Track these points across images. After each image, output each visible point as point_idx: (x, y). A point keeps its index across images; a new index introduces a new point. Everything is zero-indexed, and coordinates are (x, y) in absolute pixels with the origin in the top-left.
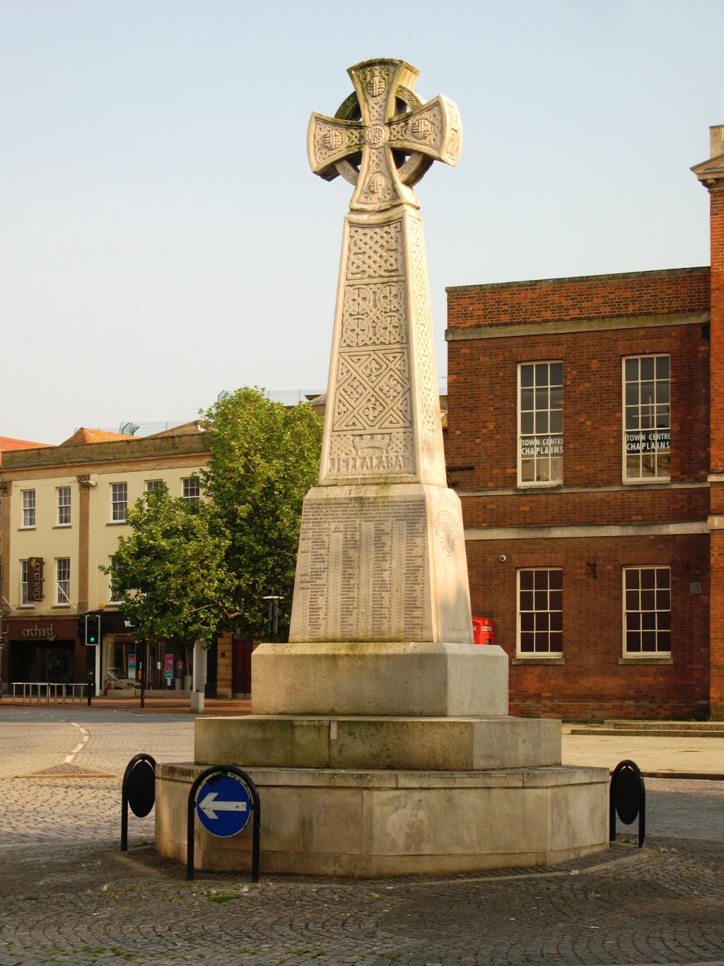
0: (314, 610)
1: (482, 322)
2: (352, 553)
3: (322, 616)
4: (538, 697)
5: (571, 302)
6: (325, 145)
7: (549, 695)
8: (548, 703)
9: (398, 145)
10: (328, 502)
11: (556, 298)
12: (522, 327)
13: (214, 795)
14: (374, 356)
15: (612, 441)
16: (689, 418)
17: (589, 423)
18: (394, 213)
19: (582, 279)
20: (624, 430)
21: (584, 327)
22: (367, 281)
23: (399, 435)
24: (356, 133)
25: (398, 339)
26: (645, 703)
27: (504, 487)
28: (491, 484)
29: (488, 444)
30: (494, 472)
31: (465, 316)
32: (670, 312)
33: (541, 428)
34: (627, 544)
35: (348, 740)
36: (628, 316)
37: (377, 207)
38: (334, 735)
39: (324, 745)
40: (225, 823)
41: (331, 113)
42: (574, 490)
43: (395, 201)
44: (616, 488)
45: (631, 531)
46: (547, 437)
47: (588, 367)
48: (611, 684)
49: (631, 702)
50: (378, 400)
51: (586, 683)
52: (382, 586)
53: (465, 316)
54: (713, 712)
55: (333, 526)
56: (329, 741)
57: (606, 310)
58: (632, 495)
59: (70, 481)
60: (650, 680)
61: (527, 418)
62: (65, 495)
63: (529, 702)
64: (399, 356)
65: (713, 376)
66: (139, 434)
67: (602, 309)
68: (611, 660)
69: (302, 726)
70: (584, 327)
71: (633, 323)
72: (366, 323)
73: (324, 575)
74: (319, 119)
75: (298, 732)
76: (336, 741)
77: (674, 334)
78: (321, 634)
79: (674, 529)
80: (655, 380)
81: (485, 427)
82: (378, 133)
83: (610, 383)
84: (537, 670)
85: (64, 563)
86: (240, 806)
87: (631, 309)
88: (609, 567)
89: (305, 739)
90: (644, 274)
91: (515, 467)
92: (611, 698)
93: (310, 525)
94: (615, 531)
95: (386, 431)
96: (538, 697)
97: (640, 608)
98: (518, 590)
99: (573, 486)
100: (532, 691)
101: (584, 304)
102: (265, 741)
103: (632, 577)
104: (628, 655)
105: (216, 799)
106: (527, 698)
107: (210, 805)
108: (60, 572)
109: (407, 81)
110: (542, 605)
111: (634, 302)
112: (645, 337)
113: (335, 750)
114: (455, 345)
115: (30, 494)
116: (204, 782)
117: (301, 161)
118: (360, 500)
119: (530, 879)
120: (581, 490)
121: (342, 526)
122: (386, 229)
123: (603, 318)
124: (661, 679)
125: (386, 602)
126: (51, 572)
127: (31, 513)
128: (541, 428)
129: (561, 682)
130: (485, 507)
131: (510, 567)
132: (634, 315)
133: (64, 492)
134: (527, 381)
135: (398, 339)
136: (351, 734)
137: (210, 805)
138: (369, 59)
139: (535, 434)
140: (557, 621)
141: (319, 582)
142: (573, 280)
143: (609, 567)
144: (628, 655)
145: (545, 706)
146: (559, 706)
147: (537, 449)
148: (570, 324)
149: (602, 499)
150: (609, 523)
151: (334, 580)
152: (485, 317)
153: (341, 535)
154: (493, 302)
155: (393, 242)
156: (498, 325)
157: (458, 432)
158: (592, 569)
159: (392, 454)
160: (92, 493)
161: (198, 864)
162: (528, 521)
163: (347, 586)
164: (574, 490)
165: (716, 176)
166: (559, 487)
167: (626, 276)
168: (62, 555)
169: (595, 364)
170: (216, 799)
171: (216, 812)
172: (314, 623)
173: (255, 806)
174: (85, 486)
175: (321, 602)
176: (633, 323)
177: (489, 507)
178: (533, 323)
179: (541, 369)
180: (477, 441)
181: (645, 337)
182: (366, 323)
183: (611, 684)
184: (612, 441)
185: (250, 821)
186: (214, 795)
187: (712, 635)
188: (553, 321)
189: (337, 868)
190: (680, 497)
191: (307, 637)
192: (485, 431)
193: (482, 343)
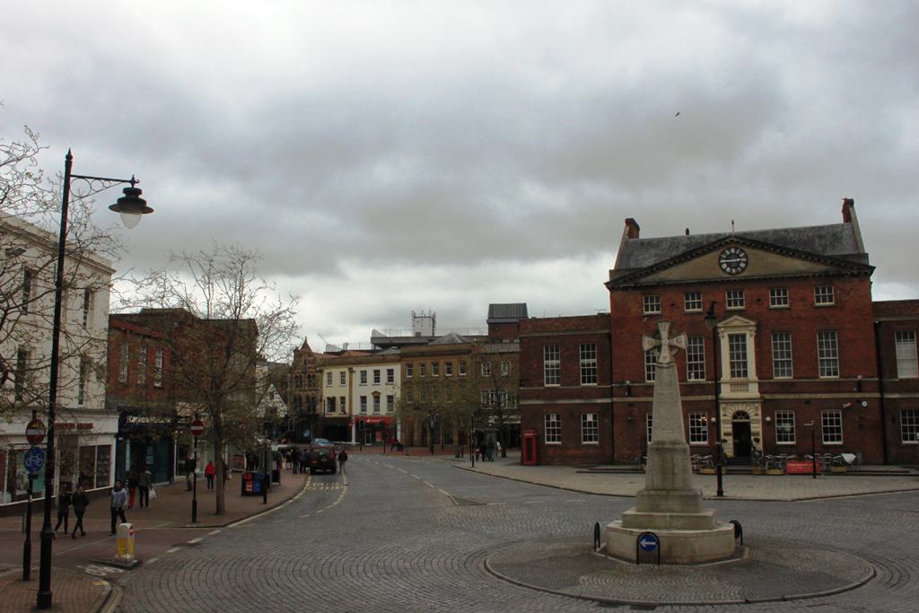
21: (566, 334)
40: (649, 548)
59: (346, 370)
66: (349, 348)
79: (599, 401)
85: (343, 399)
86: (654, 543)
107: (644, 543)
115: (330, 375)
119: (93, 465)
126: (338, 402)
127: (330, 381)
133: (343, 374)
134: (547, 351)
137: (644, 543)
138: (73, 164)
160: (354, 375)
168: (343, 395)
173: (658, 543)
174: (351, 371)
185: (657, 548)
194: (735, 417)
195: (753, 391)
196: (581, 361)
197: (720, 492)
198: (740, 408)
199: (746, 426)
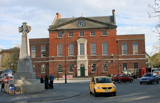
6: (20, 30)
18: (26, 36)
41: (20, 27)
43: (26, 34)
45: (42, 62)
62: (60, 46)
74: (19, 27)
79: (46, 61)
82: (25, 29)
86: (13, 88)
94: (41, 62)
97: (122, 53)
108: (80, 51)
109: (27, 24)
117: (18, 30)
158: (38, 65)
161: (9, 93)
196: (41, 51)
198: (82, 63)
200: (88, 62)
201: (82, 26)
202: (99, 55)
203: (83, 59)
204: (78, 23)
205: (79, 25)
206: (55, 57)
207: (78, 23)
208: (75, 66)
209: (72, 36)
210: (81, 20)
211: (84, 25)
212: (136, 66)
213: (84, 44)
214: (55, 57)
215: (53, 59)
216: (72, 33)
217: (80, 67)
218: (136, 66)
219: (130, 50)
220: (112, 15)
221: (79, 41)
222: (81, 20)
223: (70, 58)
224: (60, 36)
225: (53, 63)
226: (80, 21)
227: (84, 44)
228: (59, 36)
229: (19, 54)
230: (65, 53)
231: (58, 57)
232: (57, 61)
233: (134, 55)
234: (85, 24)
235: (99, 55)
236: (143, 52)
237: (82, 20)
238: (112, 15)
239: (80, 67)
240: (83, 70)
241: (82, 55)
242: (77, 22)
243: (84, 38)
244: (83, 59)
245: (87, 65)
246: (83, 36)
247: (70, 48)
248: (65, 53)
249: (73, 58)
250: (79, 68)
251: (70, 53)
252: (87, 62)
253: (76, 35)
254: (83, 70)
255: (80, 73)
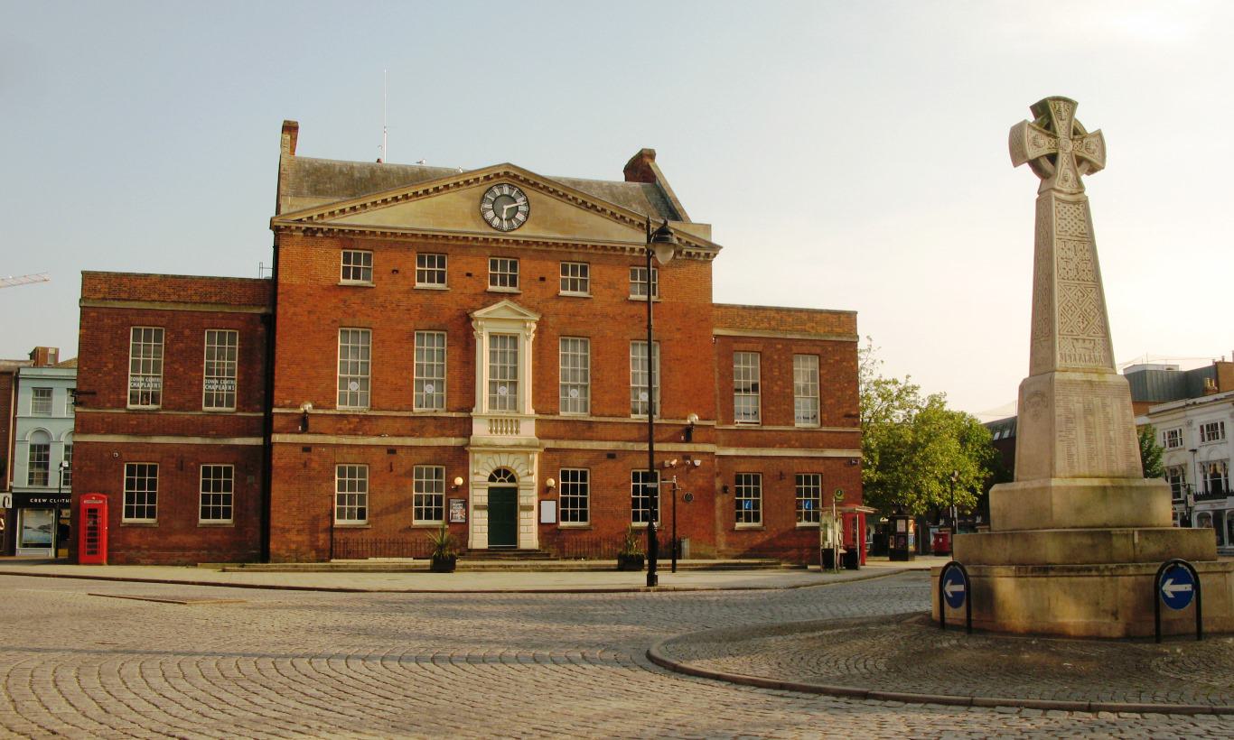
0: (1070, 456)
1: (107, 296)
2: (1089, 418)
3: (1076, 460)
4: (138, 548)
5: (172, 291)
7: (146, 547)
8: (146, 552)
9: (1080, 154)
10: (1071, 382)
11: (162, 287)
12: (137, 303)
13: (1170, 581)
14: (1079, 288)
15: (197, 382)
16: (250, 371)
17: (181, 369)
19: (180, 277)
20: (205, 376)
21: (181, 307)
22: (1069, 238)
23: (1099, 341)
24: (1053, 140)
25: (1092, 278)
26: (215, 552)
27: (118, 408)
28: (108, 405)
29: (107, 378)
30: (112, 397)
31: (95, 291)
32: (239, 305)
33: (146, 370)
34: (205, 449)
35: (1146, 543)
36: (212, 304)
37: (1069, 190)
38: (1136, 540)
39: (1131, 547)
42: (170, 412)
44: (199, 413)
45: (208, 441)
46: (223, 379)
47: (182, 333)
48: (190, 540)
49: (205, 552)
50: (1084, 317)
51: (174, 539)
52: (1110, 440)
53: (95, 291)
54: (272, 557)
55: (1075, 399)
56: (1134, 544)
57: (196, 298)
58: (209, 418)
60: (218, 537)
61: (136, 363)
63: (132, 552)
64: (1094, 290)
65: (277, 347)
67: (194, 298)
68: (192, 527)
69: (1116, 534)
70: (181, 307)
71: (215, 309)
72: (1072, 265)
73: (1074, 432)
75: (1114, 539)
76: (1138, 544)
77: (242, 318)
78: (1076, 472)
80: (216, 346)
81: (106, 366)
83: (197, 345)
84: (139, 530)
86: (1187, 587)
87: (213, 300)
88: (192, 464)
89: (1119, 543)
90: (224, 278)
91: (126, 394)
92: (190, 549)
93: (1061, 397)
94: (198, 440)
95: (1091, 338)
96: (138, 548)
98: (125, 477)
99: (169, 409)
100: (134, 545)
101: (182, 293)
102: (1093, 546)
103: (206, 470)
104: (125, 520)
105: (1173, 583)
106: (131, 549)
107: (950, 588)
110: (141, 486)
111: (216, 295)
112: (223, 318)
113: (1138, 549)
114: (86, 310)
116: (1164, 572)
118: (1091, 383)
120: (174, 413)
121: (1081, 399)
122: (1077, 206)
123: (195, 303)
124: (225, 537)
125: (1113, 451)
128: (146, 370)
129: (156, 538)
130: (103, 419)
131: (120, 461)
132: (216, 303)
134: (137, 338)
135: (1092, 278)
136: (1147, 539)
137: (950, 588)
139: (141, 374)
140: (152, 498)
141: (1071, 436)
142: (174, 277)
143: (192, 464)
144: (125, 520)
145: (143, 554)
146: (154, 555)
147: (142, 385)
148: (172, 304)
149: (188, 420)
150: (193, 435)
151: (1080, 431)
152: (109, 293)
153: (1081, 405)
154: (115, 284)
155: (1081, 215)
156: (119, 300)
157: (85, 368)
158: (181, 466)
159: (1097, 354)
162: (135, 431)
163: (1089, 441)
164: (170, 412)
165: (286, 225)
166: (158, 410)
167: (211, 278)
169: (187, 332)
170: (1173, 583)
171: (1173, 593)
172: (1071, 465)
173: (1197, 586)
175: (1074, 450)
176: (215, 309)
177: (106, 420)
178: (144, 301)
179: (158, 333)
180: (100, 375)
181: (223, 318)
182: (1072, 265)
183: (190, 540)
184: (197, 382)
186: (949, 581)
187: (272, 509)
188: (159, 301)
189: (1214, 627)
190: (242, 421)
191: (1067, 475)
192: (105, 369)
193: (104, 310)
194: (492, 479)
195: (528, 431)
197: (652, 580)
198: (504, 461)
199: (513, 493)
200: (542, 456)
201: (505, 225)
202: (611, 420)
203: (506, 434)
204: (483, 199)
205: (490, 215)
206: (321, 412)
207: (483, 199)
208: (459, 481)
209: (441, 280)
210: (500, 186)
211: (520, 217)
212: (141, 486)
213: (515, 338)
214: (321, 412)
215: (304, 422)
216: (442, 264)
217: (490, 489)
218: (217, 488)
219: (776, 400)
220: (268, 274)
221: (489, 322)
222: (500, 186)
223: (420, 425)
224: (357, 271)
225: (299, 450)
226: (506, 190)
227: (515, 338)
228: (346, 270)
229: (1051, 222)
230: (391, 384)
231: (342, 416)
232: (333, 440)
233: (799, 431)
234: (527, 215)
235: (611, 420)
236: (848, 416)
237: (511, 187)
238: (268, 274)
239: (490, 489)
240: (504, 507)
241: (497, 412)
242: (477, 190)
243: (523, 305)
244: (506, 434)
245: (535, 479)
246: (508, 289)
247: (428, 356)
248: (391, 384)
249: (441, 426)
250: (479, 496)
251: (428, 397)
252: (536, 458)
253: (469, 275)
254: (504, 507)
255: (486, 528)
